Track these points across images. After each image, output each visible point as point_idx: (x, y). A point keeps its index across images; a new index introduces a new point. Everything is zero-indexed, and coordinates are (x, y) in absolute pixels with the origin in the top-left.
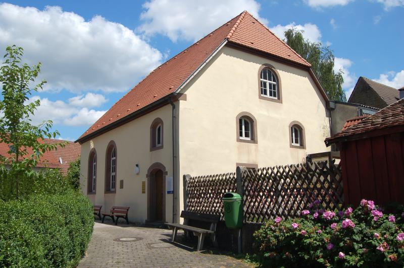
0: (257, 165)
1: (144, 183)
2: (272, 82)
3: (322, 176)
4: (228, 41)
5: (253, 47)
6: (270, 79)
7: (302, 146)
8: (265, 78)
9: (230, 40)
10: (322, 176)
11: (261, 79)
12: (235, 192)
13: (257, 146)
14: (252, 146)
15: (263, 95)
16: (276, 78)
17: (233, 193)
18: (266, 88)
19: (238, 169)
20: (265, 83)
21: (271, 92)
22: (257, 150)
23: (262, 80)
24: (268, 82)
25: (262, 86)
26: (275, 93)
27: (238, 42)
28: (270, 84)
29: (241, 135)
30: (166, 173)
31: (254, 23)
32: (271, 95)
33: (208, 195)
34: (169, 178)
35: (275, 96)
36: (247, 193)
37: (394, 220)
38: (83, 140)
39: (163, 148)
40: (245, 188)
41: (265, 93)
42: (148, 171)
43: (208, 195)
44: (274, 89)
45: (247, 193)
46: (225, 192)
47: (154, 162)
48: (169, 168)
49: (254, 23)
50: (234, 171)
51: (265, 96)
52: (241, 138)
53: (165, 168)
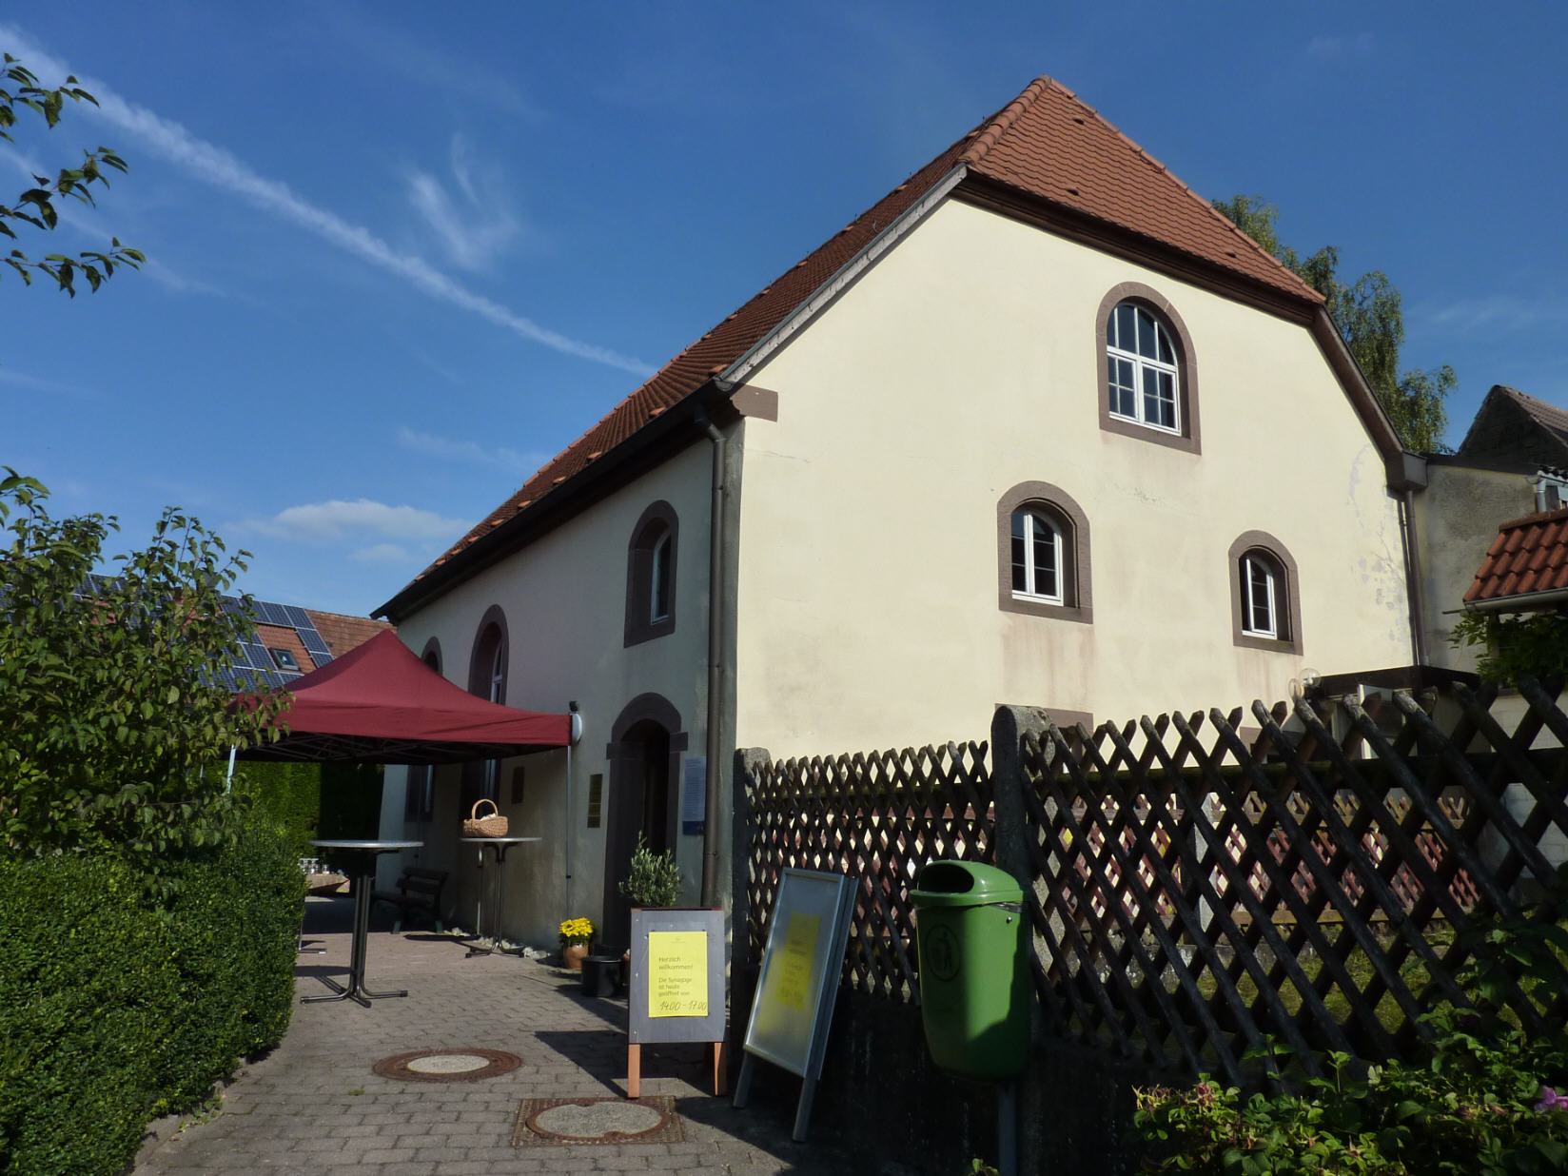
0: (1089, 717)
1: (597, 780)
2: (1159, 366)
3: (1051, 799)
4: (968, 170)
5: (1076, 205)
6: (1147, 351)
7: (1288, 640)
8: (1127, 344)
9: (979, 169)
10: (1051, 799)
11: (1109, 348)
12: (986, 858)
13: (1091, 632)
14: (1071, 629)
15: (1115, 416)
16: (1171, 340)
17: (971, 867)
18: (1131, 385)
19: (1004, 718)
20: (1126, 368)
21: (1150, 405)
22: (1088, 650)
23: (1116, 352)
24: (1139, 362)
25: (1112, 379)
26: (1169, 409)
27: (1011, 179)
28: (1149, 374)
29: (1019, 583)
30: (683, 741)
31: (1080, 122)
32: (1151, 416)
33: (868, 838)
34: (692, 756)
35: (1170, 423)
36: (1054, 864)
37: (64, 537)
38: (403, 607)
39: (672, 631)
40: (1042, 837)
41: (1128, 409)
42: (615, 729)
43: (868, 838)
44: (1167, 392)
45: (1054, 864)
46: (930, 849)
47: (637, 691)
48: (693, 722)
49: (1080, 122)
50: (983, 734)
51: (1126, 419)
52: (1017, 595)
53: (676, 716)
